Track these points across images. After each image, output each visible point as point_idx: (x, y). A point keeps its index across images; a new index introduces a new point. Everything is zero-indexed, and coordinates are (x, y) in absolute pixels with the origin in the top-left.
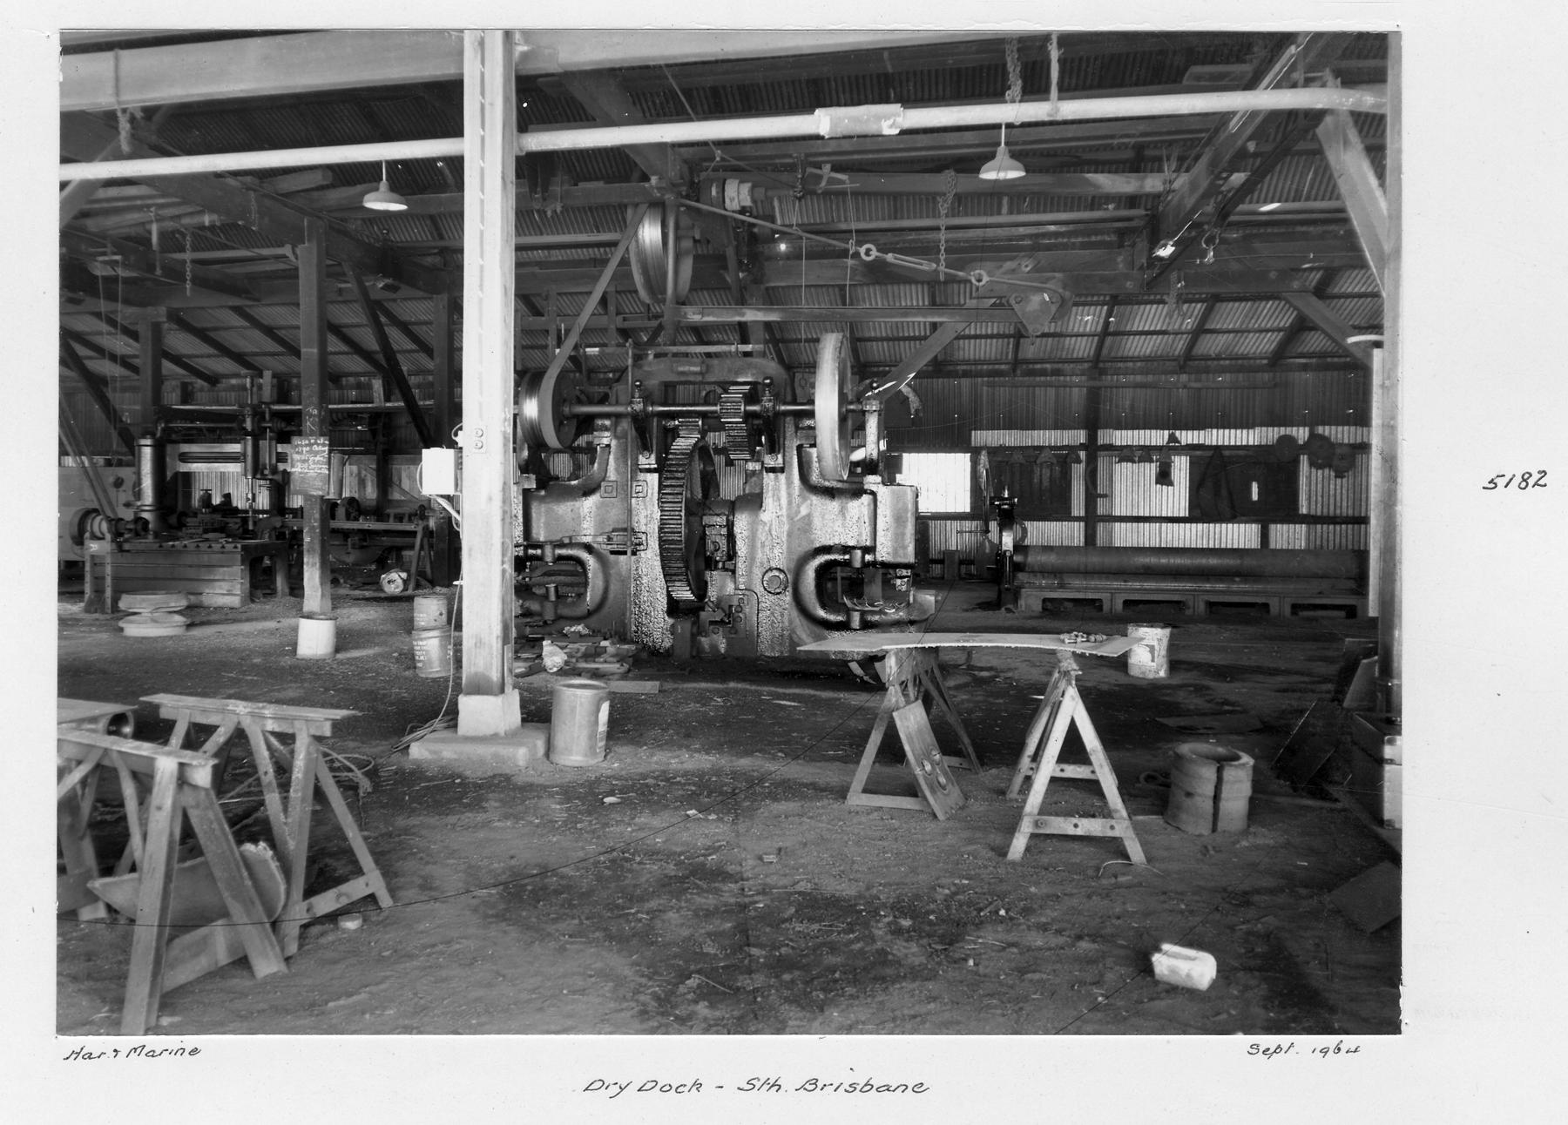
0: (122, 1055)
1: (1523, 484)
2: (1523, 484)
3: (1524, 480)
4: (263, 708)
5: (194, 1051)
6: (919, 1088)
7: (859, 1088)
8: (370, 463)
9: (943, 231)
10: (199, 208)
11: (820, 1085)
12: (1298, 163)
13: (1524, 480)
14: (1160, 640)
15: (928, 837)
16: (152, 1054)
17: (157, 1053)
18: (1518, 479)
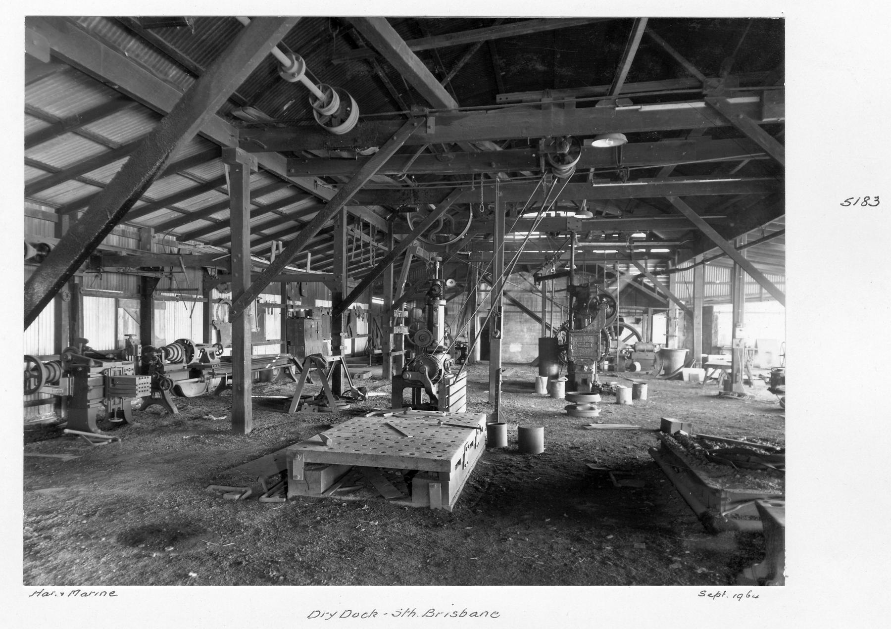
0: (65, 595)
1: (865, 203)
2: (865, 203)
3: (865, 201)
4: (719, 404)
5: (112, 594)
6: (495, 615)
7: (459, 614)
8: (133, 306)
9: (482, 177)
10: (64, 233)
11: (436, 613)
12: (52, 84)
13: (865, 201)
14: (136, 312)
15: (142, 449)
16: (86, 595)
17: (50, 593)
18: (862, 200)
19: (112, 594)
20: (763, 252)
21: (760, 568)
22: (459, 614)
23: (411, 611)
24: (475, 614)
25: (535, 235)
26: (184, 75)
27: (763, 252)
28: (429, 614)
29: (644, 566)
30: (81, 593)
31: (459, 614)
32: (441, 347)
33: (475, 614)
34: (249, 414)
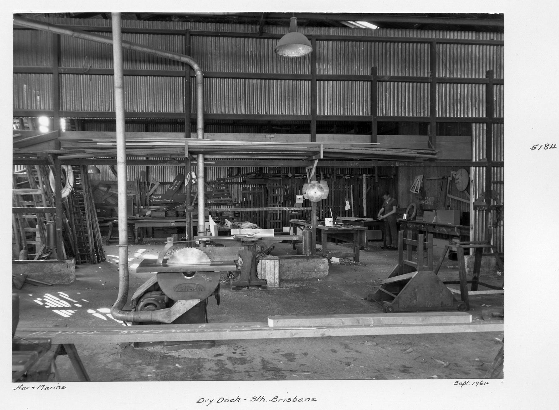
11: (278, 399)
18: (544, 146)
19: (64, 387)
20: (499, 175)
21: (70, 128)
22: (292, 400)
23: (262, 397)
24: (301, 400)
25: (449, 267)
26: (186, 29)
27: (499, 175)
28: (274, 400)
29: (128, 355)
30: (45, 387)
31: (292, 400)
32: (337, 218)
33: (301, 400)
34: (122, 220)
